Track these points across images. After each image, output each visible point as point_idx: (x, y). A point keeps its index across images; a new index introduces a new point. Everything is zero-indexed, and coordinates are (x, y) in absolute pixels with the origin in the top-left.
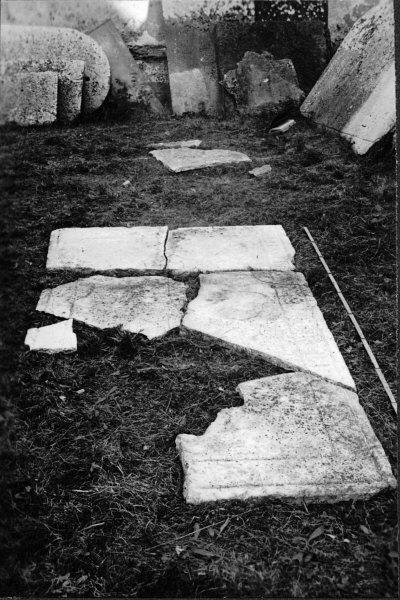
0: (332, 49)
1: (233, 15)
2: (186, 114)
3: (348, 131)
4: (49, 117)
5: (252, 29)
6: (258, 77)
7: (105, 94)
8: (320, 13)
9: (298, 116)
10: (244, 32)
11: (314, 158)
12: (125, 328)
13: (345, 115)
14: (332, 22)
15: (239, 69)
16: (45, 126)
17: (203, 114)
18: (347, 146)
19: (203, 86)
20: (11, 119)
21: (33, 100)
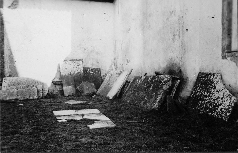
0: (102, 81)
1: (78, 74)
2: (69, 96)
3: (108, 96)
4: (36, 97)
5: (83, 77)
6: (85, 87)
7: (47, 93)
8: (99, 73)
9: (96, 95)
10: (81, 77)
11: (101, 100)
12: (74, 119)
13: (107, 93)
14: (102, 75)
15: (81, 86)
16: (35, 99)
17: (73, 95)
18: (108, 98)
19: (72, 90)
20: (26, 98)
21: (31, 94)
